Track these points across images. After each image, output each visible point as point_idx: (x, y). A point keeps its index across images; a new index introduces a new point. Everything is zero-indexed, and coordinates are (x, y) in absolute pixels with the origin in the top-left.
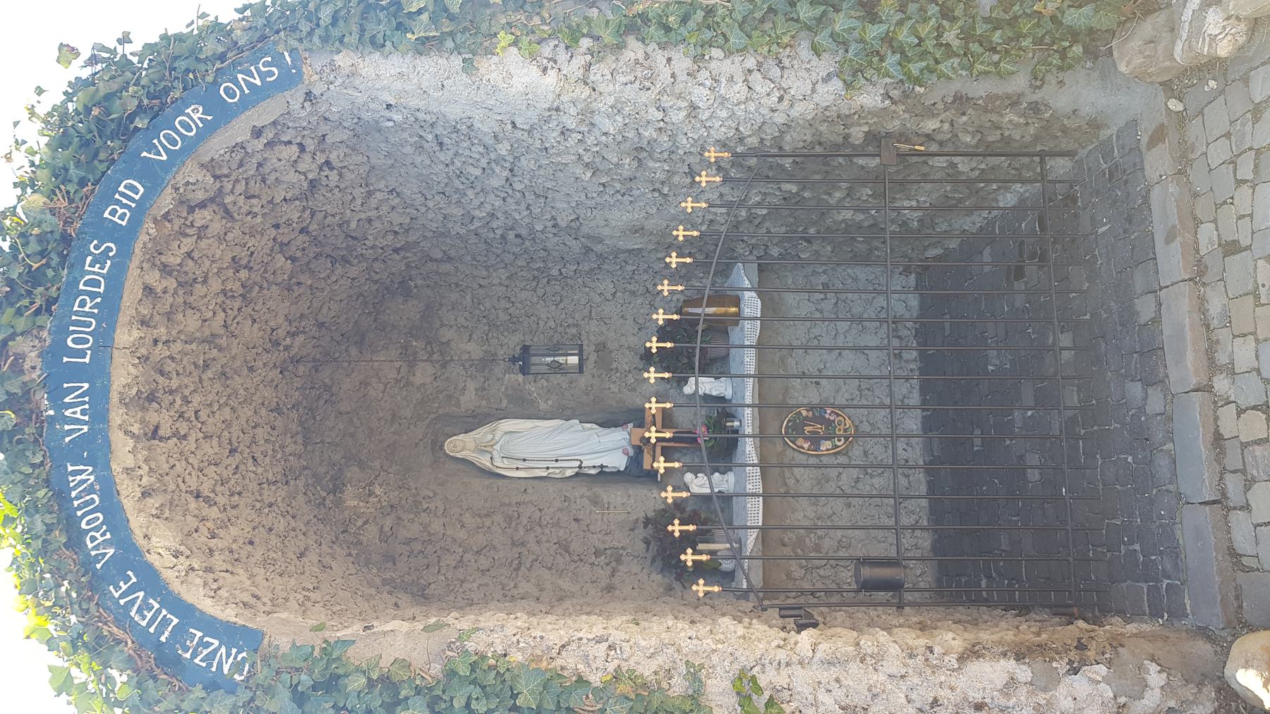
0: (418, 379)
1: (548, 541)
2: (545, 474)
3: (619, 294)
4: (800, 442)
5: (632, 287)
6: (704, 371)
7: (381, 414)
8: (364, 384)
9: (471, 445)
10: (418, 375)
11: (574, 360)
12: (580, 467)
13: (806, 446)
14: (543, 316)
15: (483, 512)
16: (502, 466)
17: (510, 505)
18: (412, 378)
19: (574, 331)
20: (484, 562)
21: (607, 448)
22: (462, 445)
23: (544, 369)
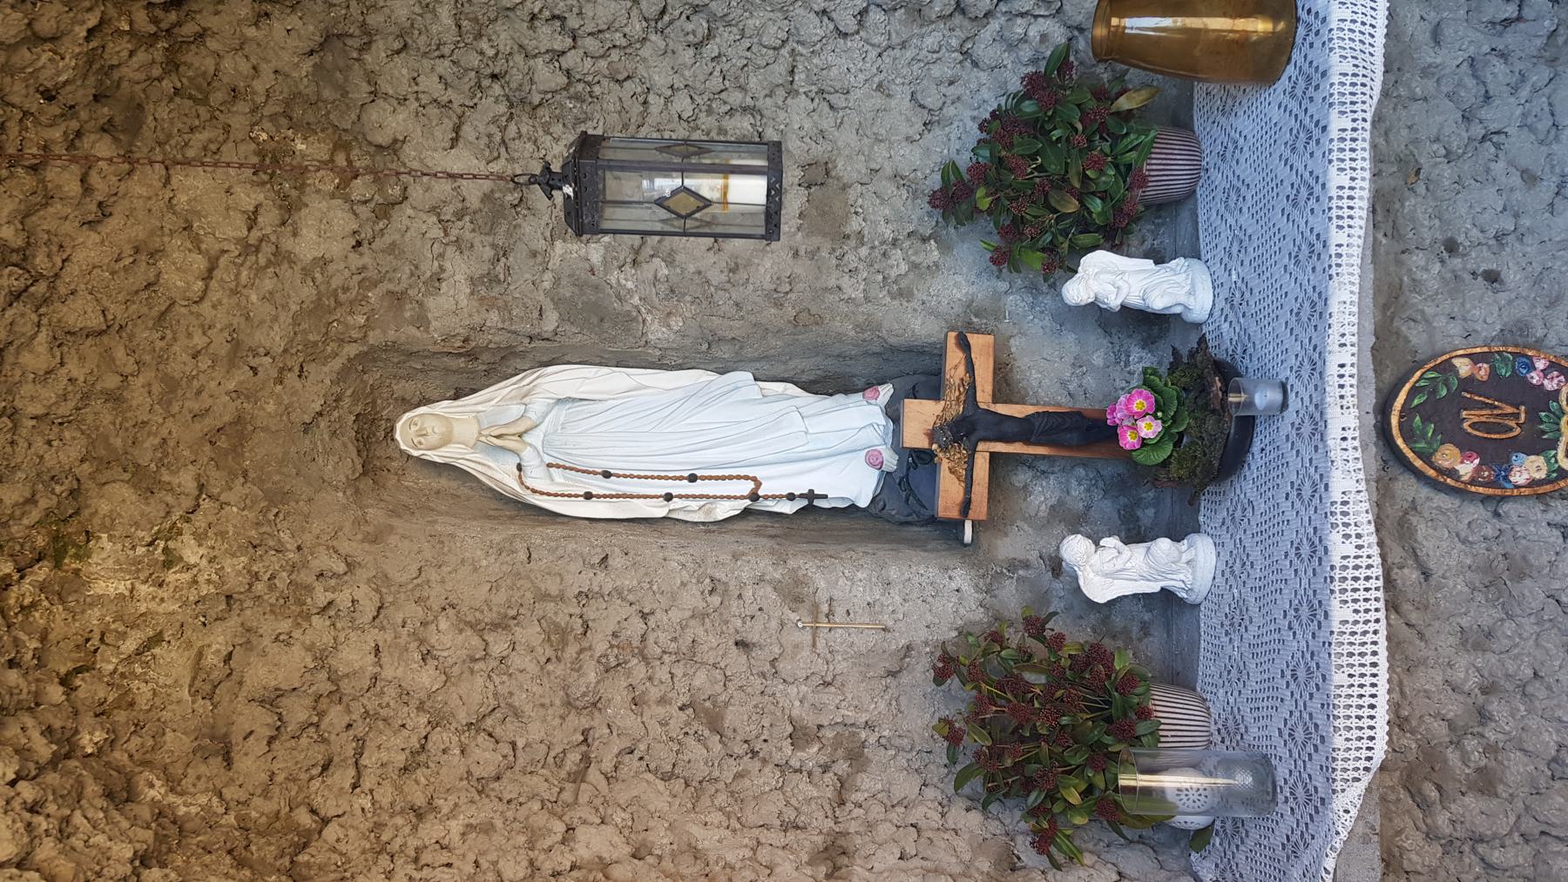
0: (307, 246)
1: (663, 701)
2: (660, 512)
3: (876, 16)
4: (1448, 456)
6: (1114, 238)
7: (199, 340)
10: (308, 233)
11: (749, 191)
12: (754, 496)
13: (1466, 469)
14: (661, 79)
15: (489, 617)
17: (561, 597)
18: (288, 243)
20: (486, 757)
21: (834, 448)
22: (438, 430)
23: (653, 218)
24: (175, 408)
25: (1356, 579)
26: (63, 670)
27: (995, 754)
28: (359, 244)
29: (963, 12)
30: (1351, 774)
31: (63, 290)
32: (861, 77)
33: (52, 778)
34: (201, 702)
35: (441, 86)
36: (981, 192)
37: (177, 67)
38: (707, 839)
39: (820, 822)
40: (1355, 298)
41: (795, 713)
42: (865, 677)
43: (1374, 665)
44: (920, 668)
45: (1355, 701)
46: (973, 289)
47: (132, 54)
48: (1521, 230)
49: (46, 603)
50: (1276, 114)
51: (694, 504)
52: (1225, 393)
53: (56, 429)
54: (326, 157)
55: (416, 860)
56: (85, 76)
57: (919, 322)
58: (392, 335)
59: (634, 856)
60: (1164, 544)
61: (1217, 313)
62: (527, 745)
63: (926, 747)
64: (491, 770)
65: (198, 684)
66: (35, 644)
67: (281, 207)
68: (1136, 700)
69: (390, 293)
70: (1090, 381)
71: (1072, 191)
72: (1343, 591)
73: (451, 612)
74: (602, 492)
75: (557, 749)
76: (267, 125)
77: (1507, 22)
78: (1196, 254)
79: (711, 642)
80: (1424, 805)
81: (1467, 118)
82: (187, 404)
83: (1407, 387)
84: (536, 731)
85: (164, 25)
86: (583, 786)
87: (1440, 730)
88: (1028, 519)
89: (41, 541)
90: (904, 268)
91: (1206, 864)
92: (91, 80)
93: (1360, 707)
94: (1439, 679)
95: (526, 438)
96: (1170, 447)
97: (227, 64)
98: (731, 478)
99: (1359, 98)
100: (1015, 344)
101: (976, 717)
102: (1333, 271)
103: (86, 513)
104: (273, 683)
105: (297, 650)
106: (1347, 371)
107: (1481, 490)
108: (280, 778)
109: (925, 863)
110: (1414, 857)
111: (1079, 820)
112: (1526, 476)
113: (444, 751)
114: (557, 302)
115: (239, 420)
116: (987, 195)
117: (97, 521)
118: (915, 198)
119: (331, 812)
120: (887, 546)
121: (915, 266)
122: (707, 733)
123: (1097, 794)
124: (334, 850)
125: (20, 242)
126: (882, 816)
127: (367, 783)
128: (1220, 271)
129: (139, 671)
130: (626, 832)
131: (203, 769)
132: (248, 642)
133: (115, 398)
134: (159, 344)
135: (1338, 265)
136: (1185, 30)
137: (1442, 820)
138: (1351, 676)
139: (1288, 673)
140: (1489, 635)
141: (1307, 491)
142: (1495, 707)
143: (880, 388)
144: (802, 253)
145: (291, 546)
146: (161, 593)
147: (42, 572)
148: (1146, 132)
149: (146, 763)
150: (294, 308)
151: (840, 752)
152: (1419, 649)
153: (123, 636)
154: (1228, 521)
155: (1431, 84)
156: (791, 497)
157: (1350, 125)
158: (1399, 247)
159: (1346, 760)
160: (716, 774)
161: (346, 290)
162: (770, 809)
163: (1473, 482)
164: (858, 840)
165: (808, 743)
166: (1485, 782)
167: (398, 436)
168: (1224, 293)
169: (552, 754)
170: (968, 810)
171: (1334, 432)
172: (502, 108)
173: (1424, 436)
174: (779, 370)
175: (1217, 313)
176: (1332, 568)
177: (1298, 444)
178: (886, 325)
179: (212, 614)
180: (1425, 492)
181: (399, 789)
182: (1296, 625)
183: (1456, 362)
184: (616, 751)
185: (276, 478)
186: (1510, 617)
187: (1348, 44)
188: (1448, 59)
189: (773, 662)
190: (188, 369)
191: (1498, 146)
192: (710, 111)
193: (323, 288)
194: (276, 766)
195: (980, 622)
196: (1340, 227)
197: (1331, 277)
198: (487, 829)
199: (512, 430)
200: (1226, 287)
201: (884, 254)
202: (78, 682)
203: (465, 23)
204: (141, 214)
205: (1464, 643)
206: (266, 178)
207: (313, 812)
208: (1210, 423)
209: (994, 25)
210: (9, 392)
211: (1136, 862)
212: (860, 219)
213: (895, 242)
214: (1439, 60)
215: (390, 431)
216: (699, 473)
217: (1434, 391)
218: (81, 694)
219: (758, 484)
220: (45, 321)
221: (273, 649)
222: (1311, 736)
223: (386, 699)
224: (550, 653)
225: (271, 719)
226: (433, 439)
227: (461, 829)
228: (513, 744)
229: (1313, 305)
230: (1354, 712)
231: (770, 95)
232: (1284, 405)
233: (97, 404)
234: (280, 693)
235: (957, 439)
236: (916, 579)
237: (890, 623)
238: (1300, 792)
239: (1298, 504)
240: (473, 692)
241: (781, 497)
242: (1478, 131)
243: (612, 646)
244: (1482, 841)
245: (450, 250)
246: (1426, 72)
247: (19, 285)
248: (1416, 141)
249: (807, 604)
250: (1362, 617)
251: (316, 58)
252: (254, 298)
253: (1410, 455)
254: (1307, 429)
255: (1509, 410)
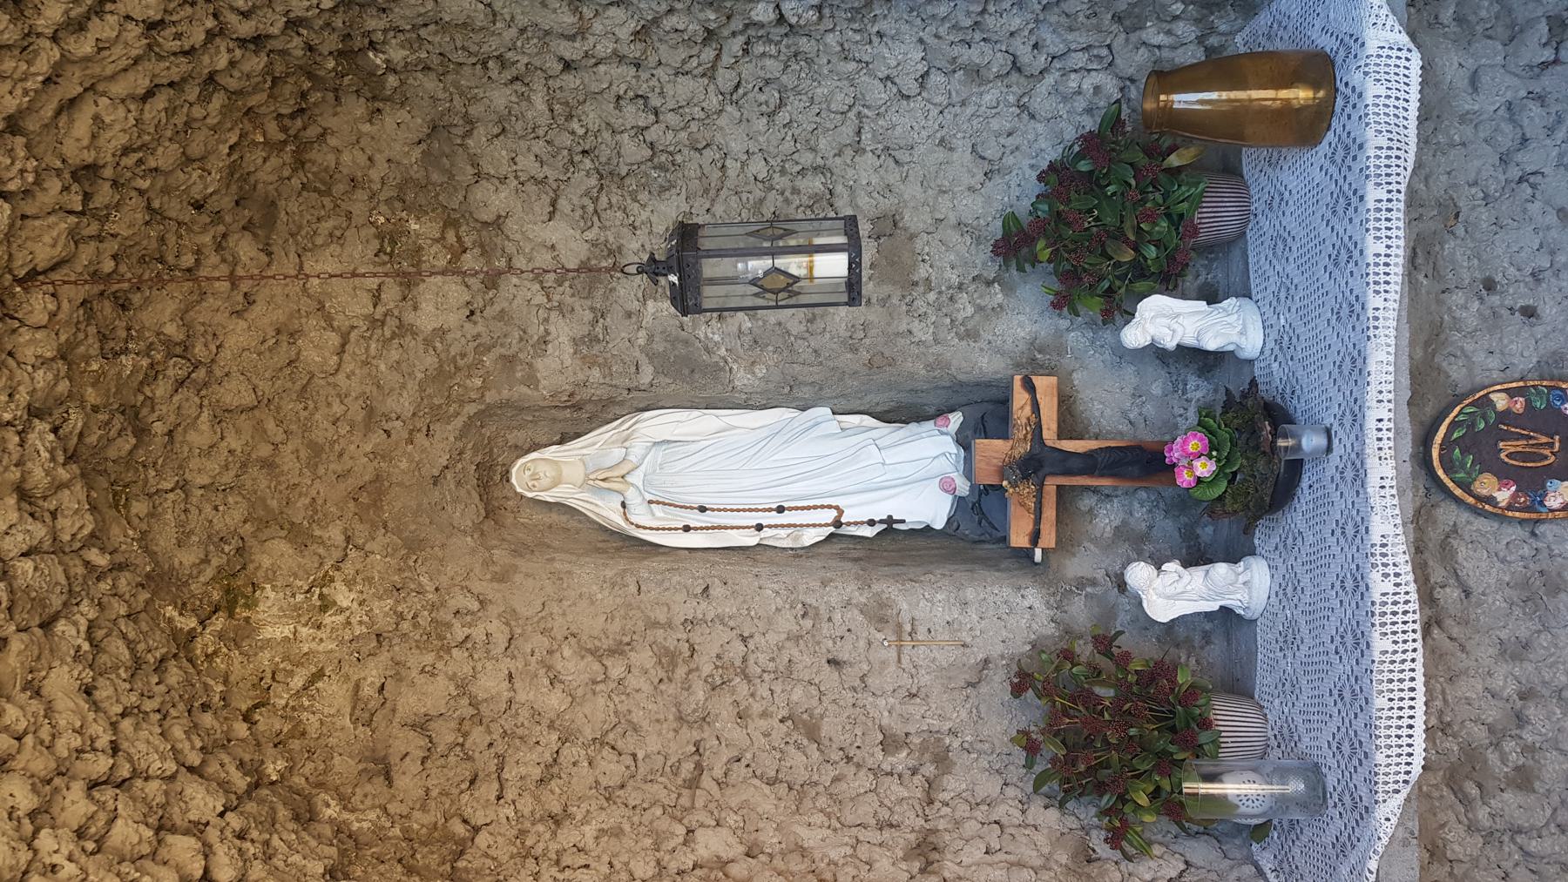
0: (427, 318)
1: (764, 714)
2: (752, 541)
3: (936, 78)
4: (1486, 484)
5: (973, 55)
6: (1169, 281)
7: (337, 409)
8: (288, 333)
9: (575, 473)
10: (427, 307)
11: (833, 266)
12: (837, 523)
13: (1503, 496)
14: (736, 146)
15: (606, 644)
16: (647, 522)
17: (669, 625)
18: (409, 317)
19: (815, 184)
20: (611, 769)
21: (911, 475)
22: (550, 474)
24: (321, 471)
25: (1394, 613)
26: (244, 708)
27: (1070, 761)
28: (472, 313)
29: (1019, 70)
30: (1392, 787)
31: (218, 373)
32: (924, 134)
33: (251, 807)
34: (361, 728)
35: (538, 165)
36: (1041, 244)
37: (303, 164)
38: (810, 838)
39: (912, 820)
40: (1391, 358)
41: (885, 722)
42: (947, 689)
43: (1412, 689)
44: (997, 678)
45: (1395, 722)
46: (1036, 327)
47: (265, 160)
48: (1556, 266)
49: (224, 650)
50: (1319, 177)
51: (783, 532)
52: (1275, 435)
53: (221, 495)
54: (438, 235)
55: (558, 862)
56: (228, 186)
57: (986, 360)
58: (505, 393)
59: (748, 855)
60: (1221, 569)
61: (1268, 352)
62: (647, 756)
63: (1006, 750)
64: (617, 781)
65: (358, 712)
66: (220, 688)
67: (401, 284)
68: (1198, 711)
69: (503, 357)
70: (1149, 409)
71: (1126, 241)
72: (1383, 625)
73: (572, 640)
74: (699, 525)
75: (673, 759)
76: (383, 208)
77: (1545, 65)
78: (1248, 295)
79: (807, 662)
80: (1465, 801)
81: (1504, 160)
82: (332, 466)
83: (1447, 421)
84: (653, 744)
85: (292, 132)
86: (698, 792)
87: (1480, 734)
88: (1094, 541)
89: (216, 596)
90: (970, 310)
91: (1265, 854)
92: (234, 188)
93: (1400, 727)
94: (1480, 687)
95: (629, 478)
96: (1225, 483)
97: (346, 158)
98: (815, 507)
99: (1394, 170)
100: (1077, 377)
101: (1052, 730)
102: (1371, 333)
103: (251, 567)
104: (423, 710)
105: (441, 681)
106: (1385, 425)
107: (1517, 514)
108: (434, 793)
109: (1008, 857)
110: (1456, 847)
111: (1148, 818)
112: (1560, 500)
113: (574, 764)
114: (651, 357)
115: (378, 478)
116: (1047, 247)
117: (260, 573)
118: (979, 244)
119: (479, 823)
120: (962, 567)
121: (980, 309)
122: (805, 742)
123: (1164, 795)
124: (486, 855)
125: (182, 337)
126: (967, 814)
127: (510, 794)
128: (1269, 313)
129: (307, 703)
130: (739, 832)
131: (369, 788)
132: (398, 673)
133: (268, 464)
134: (304, 414)
135: (1376, 328)
136: (1229, 101)
137: (1482, 814)
138: (1391, 700)
139: (1335, 692)
140: (1526, 646)
141: (1350, 531)
142: (1531, 711)
143: (950, 416)
144: (874, 301)
145: (430, 587)
146: (320, 634)
147: (219, 622)
148: (1197, 184)
149: (320, 785)
150: (420, 376)
151: (927, 756)
152: (1461, 661)
153: (291, 674)
154: (1281, 546)
155: (1468, 130)
156: (872, 523)
157: (1385, 196)
158: (1439, 287)
159: (1386, 774)
160: (815, 778)
161: (463, 355)
162: (866, 810)
163: (1510, 507)
164: (947, 837)
165: (898, 748)
166: (1523, 779)
167: (513, 481)
168: (1274, 335)
169: (669, 763)
170: (1046, 807)
171: (1373, 481)
172: (593, 181)
173: (1463, 466)
174: (856, 405)
175: (1268, 352)
176: (1373, 603)
177: (1342, 486)
178: (954, 362)
179: (365, 650)
180: (1465, 516)
181: (537, 799)
182: (1342, 651)
183: (1493, 397)
184: (725, 759)
185: (413, 527)
186: (1547, 629)
187: (1383, 119)
188: (1488, 103)
189: (862, 679)
190: (329, 435)
191: (1534, 186)
192: (783, 172)
193: (443, 356)
194: (430, 783)
195: (1053, 636)
196: (1377, 292)
197: (1369, 338)
198: (617, 833)
199: (616, 473)
200: (1276, 328)
201: (951, 299)
202: (257, 717)
203: (557, 107)
204: (279, 300)
205: (1503, 653)
206: (386, 258)
207: (465, 821)
208: (1261, 465)
209: (1050, 79)
210: (180, 467)
211: (1201, 851)
212: (927, 266)
213: (960, 287)
214: (1476, 107)
215: (506, 476)
216: (786, 505)
217: (1473, 425)
218: (261, 727)
219: (841, 512)
220: (206, 402)
221: (421, 680)
222: (1357, 751)
223: (521, 719)
224: (662, 674)
225: (424, 742)
226: (545, 482)
227: (595, 834)
228: (634, 756)
229: (1354, 361)
230: (1393, 732)
231: (839, 155)
232: (1329, 449)
233: (254, 471)
234: (429, 718)
235: (1025, 477)
236: (991, 599)
237: (968, 640)
238: (1347, 799)
239: (1342, 540)
240: (595, 714)
241: (862, 523)
242: (1515, 173)
243: (717, 667)
244: (1520, 832)
245: (554, 314)
246: (1463, 119)
247: (182, 373)
248: (1455, 186)
249: (892, 625)
250: (1401, 647)
251: (424, 146)
252: (383, 367)
253: (1450, 485)
254: (1349, 474)
255: (1544, 439)
